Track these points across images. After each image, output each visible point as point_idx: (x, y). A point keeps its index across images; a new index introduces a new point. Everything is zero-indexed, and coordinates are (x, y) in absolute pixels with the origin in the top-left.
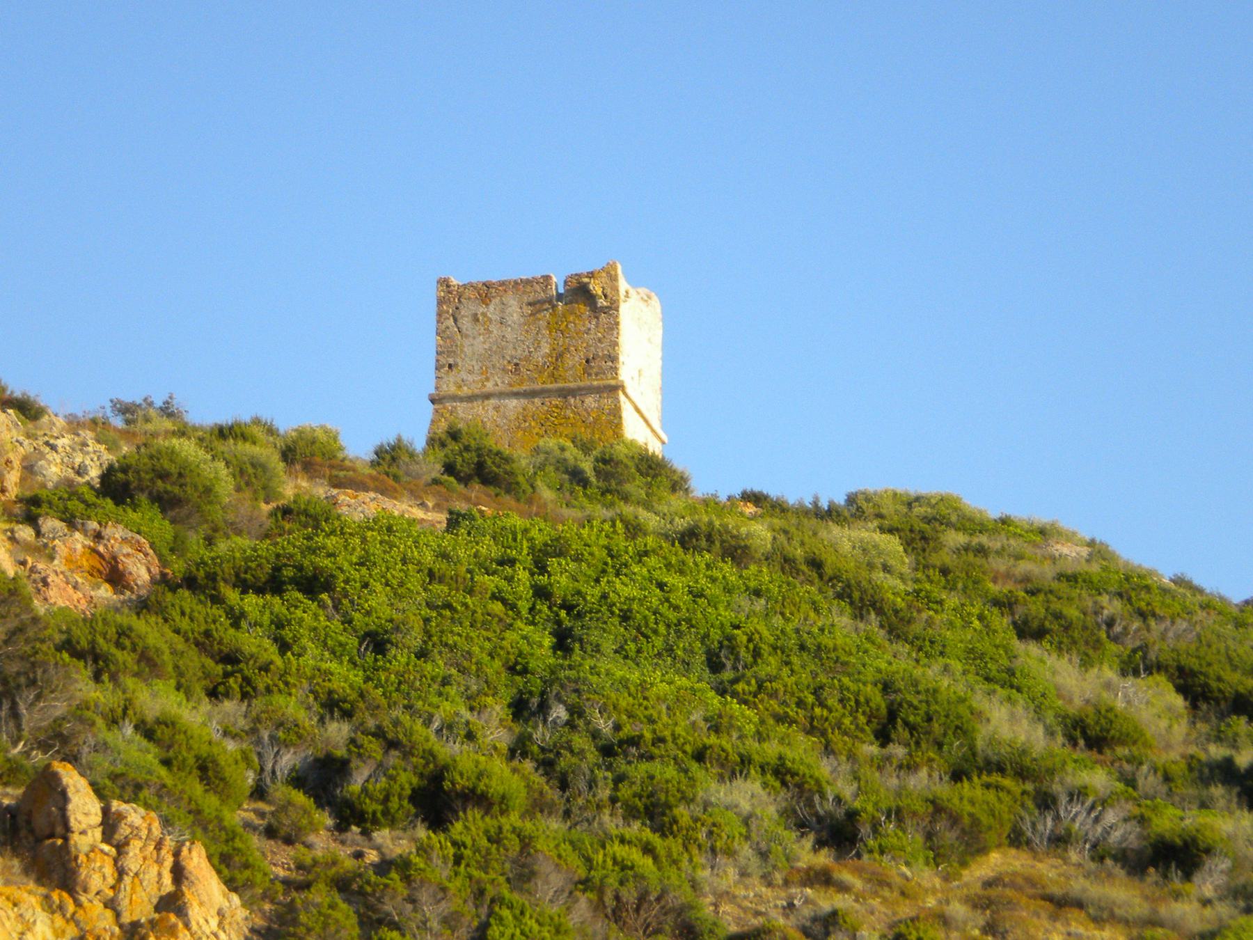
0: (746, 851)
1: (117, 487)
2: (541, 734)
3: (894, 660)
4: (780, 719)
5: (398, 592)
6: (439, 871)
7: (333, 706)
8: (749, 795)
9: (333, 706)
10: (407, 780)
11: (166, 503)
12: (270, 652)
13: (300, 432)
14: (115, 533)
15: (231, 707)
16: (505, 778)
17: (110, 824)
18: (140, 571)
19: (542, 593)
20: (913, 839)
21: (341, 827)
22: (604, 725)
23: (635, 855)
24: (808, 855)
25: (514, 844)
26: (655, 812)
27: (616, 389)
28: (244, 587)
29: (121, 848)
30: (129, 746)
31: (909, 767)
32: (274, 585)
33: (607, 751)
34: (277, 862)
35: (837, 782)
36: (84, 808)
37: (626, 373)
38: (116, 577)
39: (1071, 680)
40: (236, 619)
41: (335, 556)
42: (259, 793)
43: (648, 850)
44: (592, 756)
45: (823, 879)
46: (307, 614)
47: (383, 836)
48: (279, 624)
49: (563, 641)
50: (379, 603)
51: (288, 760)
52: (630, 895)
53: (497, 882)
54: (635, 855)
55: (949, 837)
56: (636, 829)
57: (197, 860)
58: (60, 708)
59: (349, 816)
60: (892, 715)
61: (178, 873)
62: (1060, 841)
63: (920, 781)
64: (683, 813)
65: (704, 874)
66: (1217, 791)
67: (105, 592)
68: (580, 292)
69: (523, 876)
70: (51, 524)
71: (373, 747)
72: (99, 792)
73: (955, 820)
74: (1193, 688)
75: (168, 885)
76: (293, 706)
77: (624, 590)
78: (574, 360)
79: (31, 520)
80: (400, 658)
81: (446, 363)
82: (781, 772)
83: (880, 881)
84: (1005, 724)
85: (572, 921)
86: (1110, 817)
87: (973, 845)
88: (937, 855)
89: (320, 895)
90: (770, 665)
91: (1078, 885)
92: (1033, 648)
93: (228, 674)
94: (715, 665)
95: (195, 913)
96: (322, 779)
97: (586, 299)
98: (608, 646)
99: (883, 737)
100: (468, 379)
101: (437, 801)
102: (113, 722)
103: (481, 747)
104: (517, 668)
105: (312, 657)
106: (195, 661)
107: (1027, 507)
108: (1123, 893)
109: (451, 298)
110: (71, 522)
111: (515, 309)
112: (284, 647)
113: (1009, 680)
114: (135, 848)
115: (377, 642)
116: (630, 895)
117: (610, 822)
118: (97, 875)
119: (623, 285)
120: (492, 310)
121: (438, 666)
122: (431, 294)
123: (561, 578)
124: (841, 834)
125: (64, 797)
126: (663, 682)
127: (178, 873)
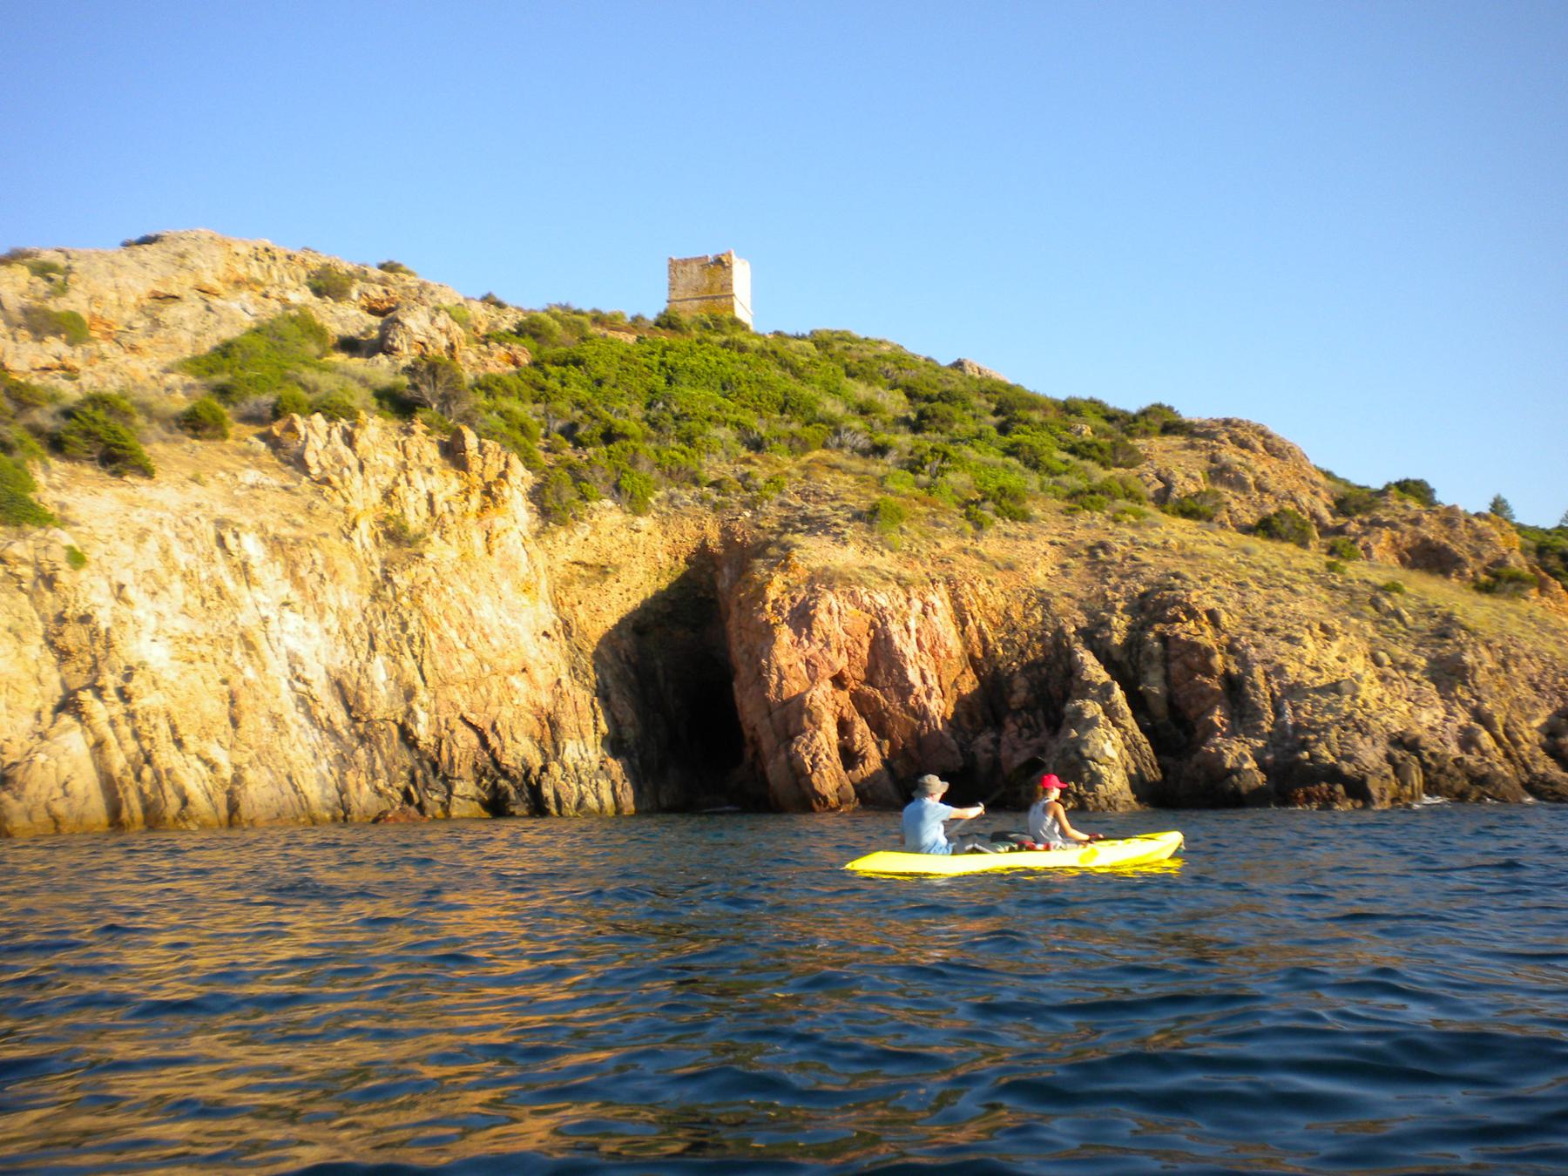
0: (721, 453)
1: (520, 331)
2: (653, 413)
3: (792, 385)
4: (744, 406)
5: (608, 365)
6: (602, 462)
7: (579, 405)
8: (726, 433)
9: (579, 405)
10: (599, 430)
11: (535, 336)
12: (558, 387)
13: (660, 315)
14: (516, 347)
15: (540, 407)
16: (633, 427)
17: (481, 447)
18: (525, 360)
19: (663, 364)
20: (784, 446)
21: (575, 447)
22: (676, 410)
23: (677, 454)
24: (744, 453)
25: (631, 451)
26: (689, 440)
27: (732, 296)
28: (554, 363)
29: (485, 455)
30: (494, 420)
31: (789, 422)
32: (565, 364)
33: (676, 418)
34: (546, 460)
35: (760, 428)
36: (471, 440)
37: (736, 289)
38: (516, 363)
39: (860, 390)
40: (547, 376)
41: (588, 351)
42: (546, 436)
43: (683, 452)
44: (671, 420)
45: (748, 461)
46: (573, 373)
47: (590, 450)
48: (563, 376)
49: (669, 381)
50: (601, 369)
51: (559, 424)
52: (675, 468)
53: (624, 465)
54: (677, 454)
55: (797, 446)
56: (682, 446)
57: (515, 460)
58: (466, 407)
59: (578, 443)
60: (786, 403)
61: (507, 464)
62: (841, 446)
63: (794, 427)
64: (699, 440)
65: (704, 461)
66: (902, 428)
67: (512, 368)
68: (719, 261)
69: (634, 462)
70: (493, 344)
71: (587, 418)
72: (479, 436)
73: (799, 439)
74: (911, 394)
75: (502, 468)
76: (564, 406)
77: (692, 362)
78: (717, 286)
79: (486, 343)
80: (606, 388)
81: (672, 288)
82: (738, 424)
83: (768, 462)
84: (832, 407)
85: (652, 478)
86: (859, 437)
87: (806, 447)
88: (792, 451)
89: (558, 471)
90: (744, 387)
91: (844, 462)
92: (850, 380)
93: (541, 394)
94: (724, 388)
95: (511, 478)
96: (569, 432)
97: (721, 264)
98: (685, 382)
99: (782, 412)
100: (680, 294)
101: (609, 437)
102: (489, 411)
103: (630, 417)
104: (652, 391)
105: (574, 387)
106: (527, 390)
107: (874, 335)
108: (857, 464)
109: (673, 265)
110: (500, 343)
111: (696, 268)
112: (563, 384)
113: (836, 391)
114: (489, 456)
115: (599, 382)
116: (675, 468)
117: (673, 444)
118: (476, 465)
119: (734, 258)
120: (687, 269)
121: (620, 390)
122: (666, 263)
123: (670, 359)
124: (757, 445)
125: (463, 438)
126: (702, 393)
127: (507, 464)
